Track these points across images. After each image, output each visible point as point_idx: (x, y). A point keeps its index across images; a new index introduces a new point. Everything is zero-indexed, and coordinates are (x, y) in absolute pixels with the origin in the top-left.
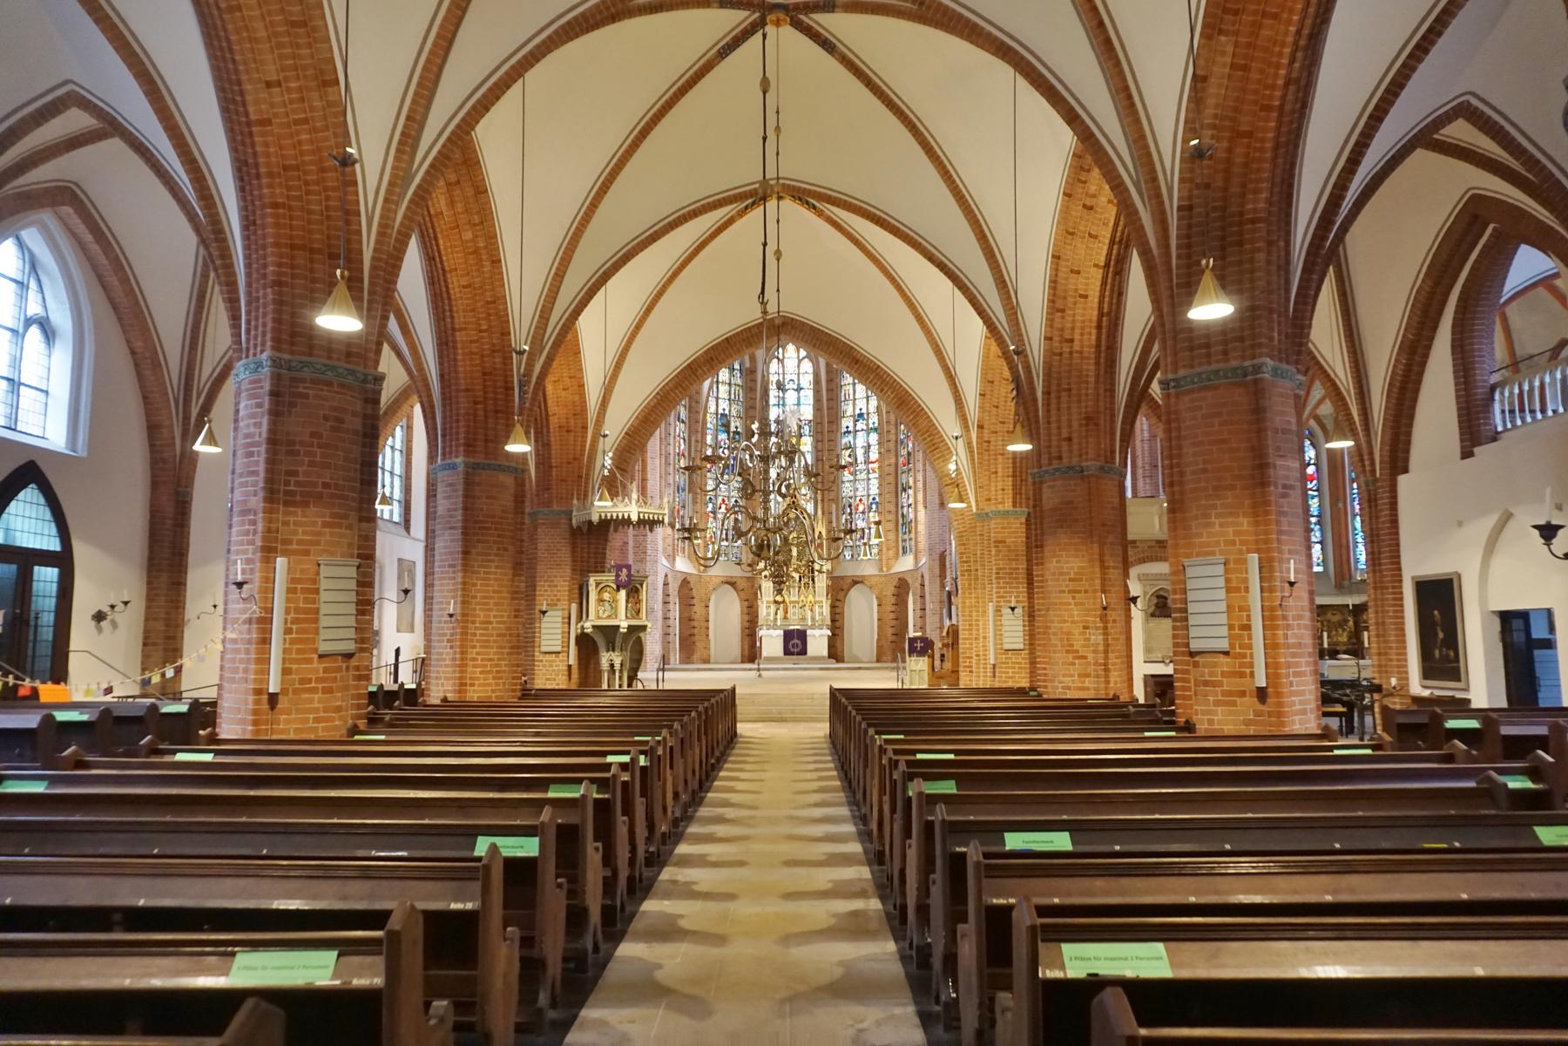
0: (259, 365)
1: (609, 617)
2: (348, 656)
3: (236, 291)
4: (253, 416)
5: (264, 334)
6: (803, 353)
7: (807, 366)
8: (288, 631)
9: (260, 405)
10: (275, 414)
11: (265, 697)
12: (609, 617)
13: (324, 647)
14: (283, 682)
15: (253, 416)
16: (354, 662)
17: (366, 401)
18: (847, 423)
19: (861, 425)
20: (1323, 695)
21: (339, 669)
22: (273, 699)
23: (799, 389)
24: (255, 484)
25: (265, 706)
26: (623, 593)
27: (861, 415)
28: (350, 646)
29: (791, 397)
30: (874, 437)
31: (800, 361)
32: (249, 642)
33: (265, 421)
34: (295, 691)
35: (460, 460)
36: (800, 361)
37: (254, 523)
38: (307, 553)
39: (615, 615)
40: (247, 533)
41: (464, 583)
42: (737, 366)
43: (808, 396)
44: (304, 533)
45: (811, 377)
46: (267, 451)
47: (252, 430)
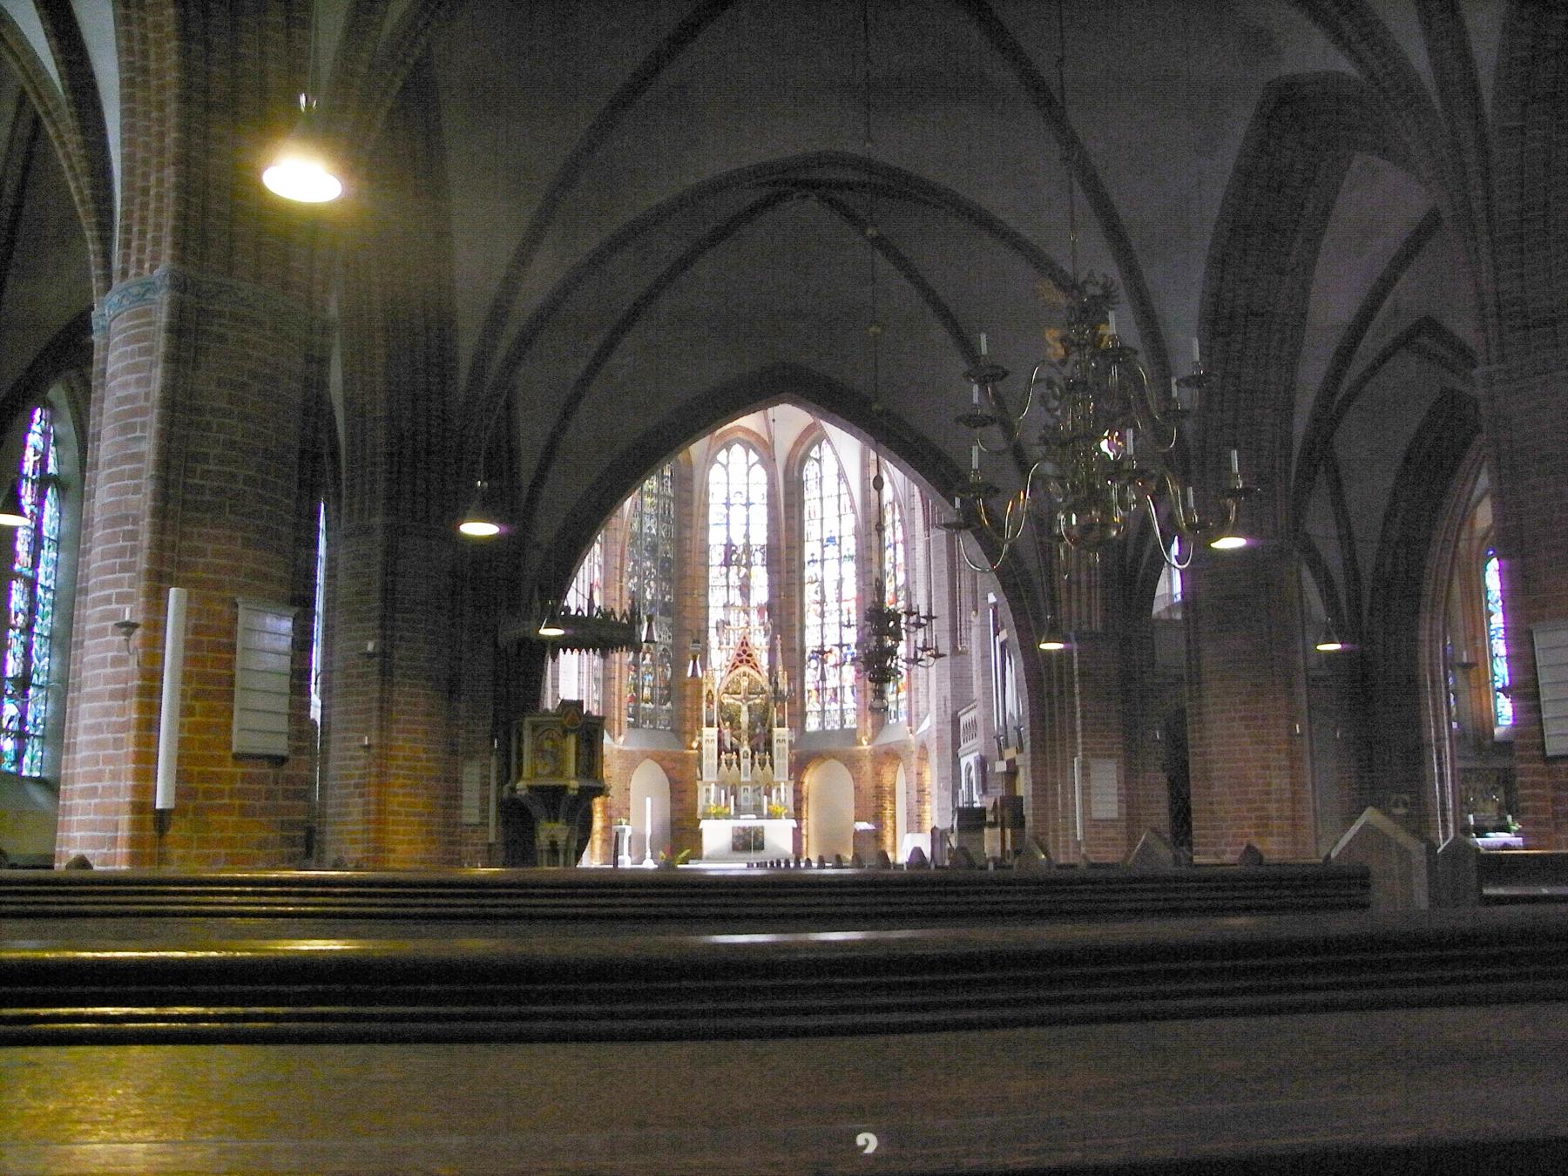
0: (150, 287)
1: (553, 773)
2: (279, 761)
3: (108, 186)
4: (133, 368)
5: (157, 241)
6: (753, 457)
7: (760, 474)
8: (186, 711)
9: (148, 351)
10: (175, 360)
11: (150, 817)
12: (553, 773)
13: (239, 742)
14: (178, 795)
15: (133, 368)
16: (287, 770)
17: (310, 359)
18: (811, 549)
19: (831, 551)
20: (1366, 886)
21: (262, 779)
22: (162, 819)
23: (748, 505)
24: (136, 474)
25: (151, 833)
26: (571, 741)
27: (831, 539)
28: (280, 746)
29: (738, 514)
30: (850, 569)
31: (749, 468)
32: (124, 727)
33: (158, 373)
34: (199, 811)
35: (378, 520)
36: (749, 468)
37: (132, 535)
38: (218, 586)
39: (558, 772)
40: (121, 553)
41: (382, 700)
42: (667, 473)
43: (760, 516)
44: (217, 554)
45: (764, 489)
46: (161, 420)
47: (132, 390)
